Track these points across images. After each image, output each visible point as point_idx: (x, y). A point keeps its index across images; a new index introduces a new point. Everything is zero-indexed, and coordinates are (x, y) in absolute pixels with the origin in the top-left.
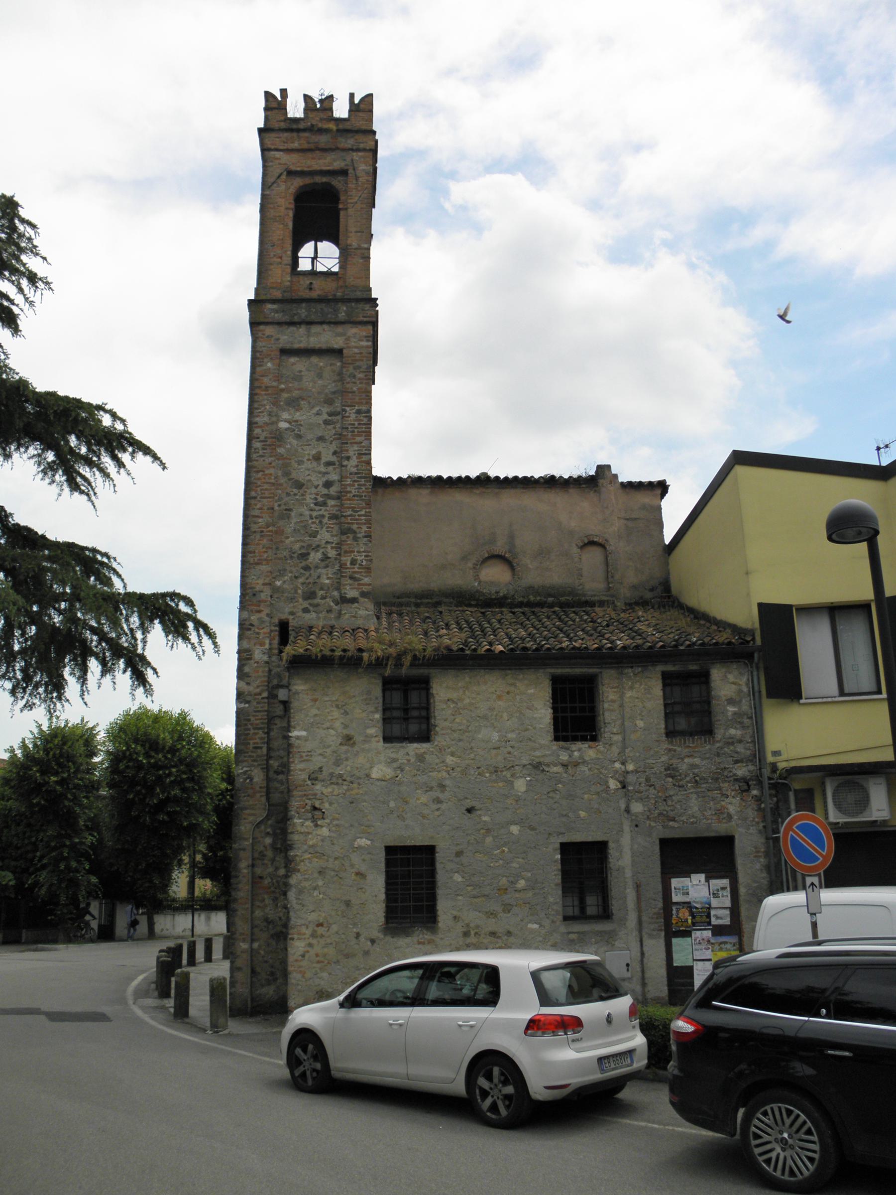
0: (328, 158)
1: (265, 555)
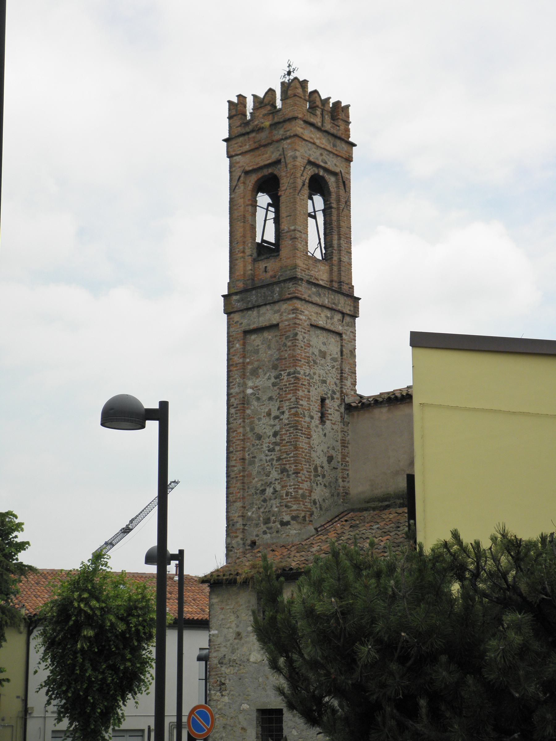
0: (269, 152)
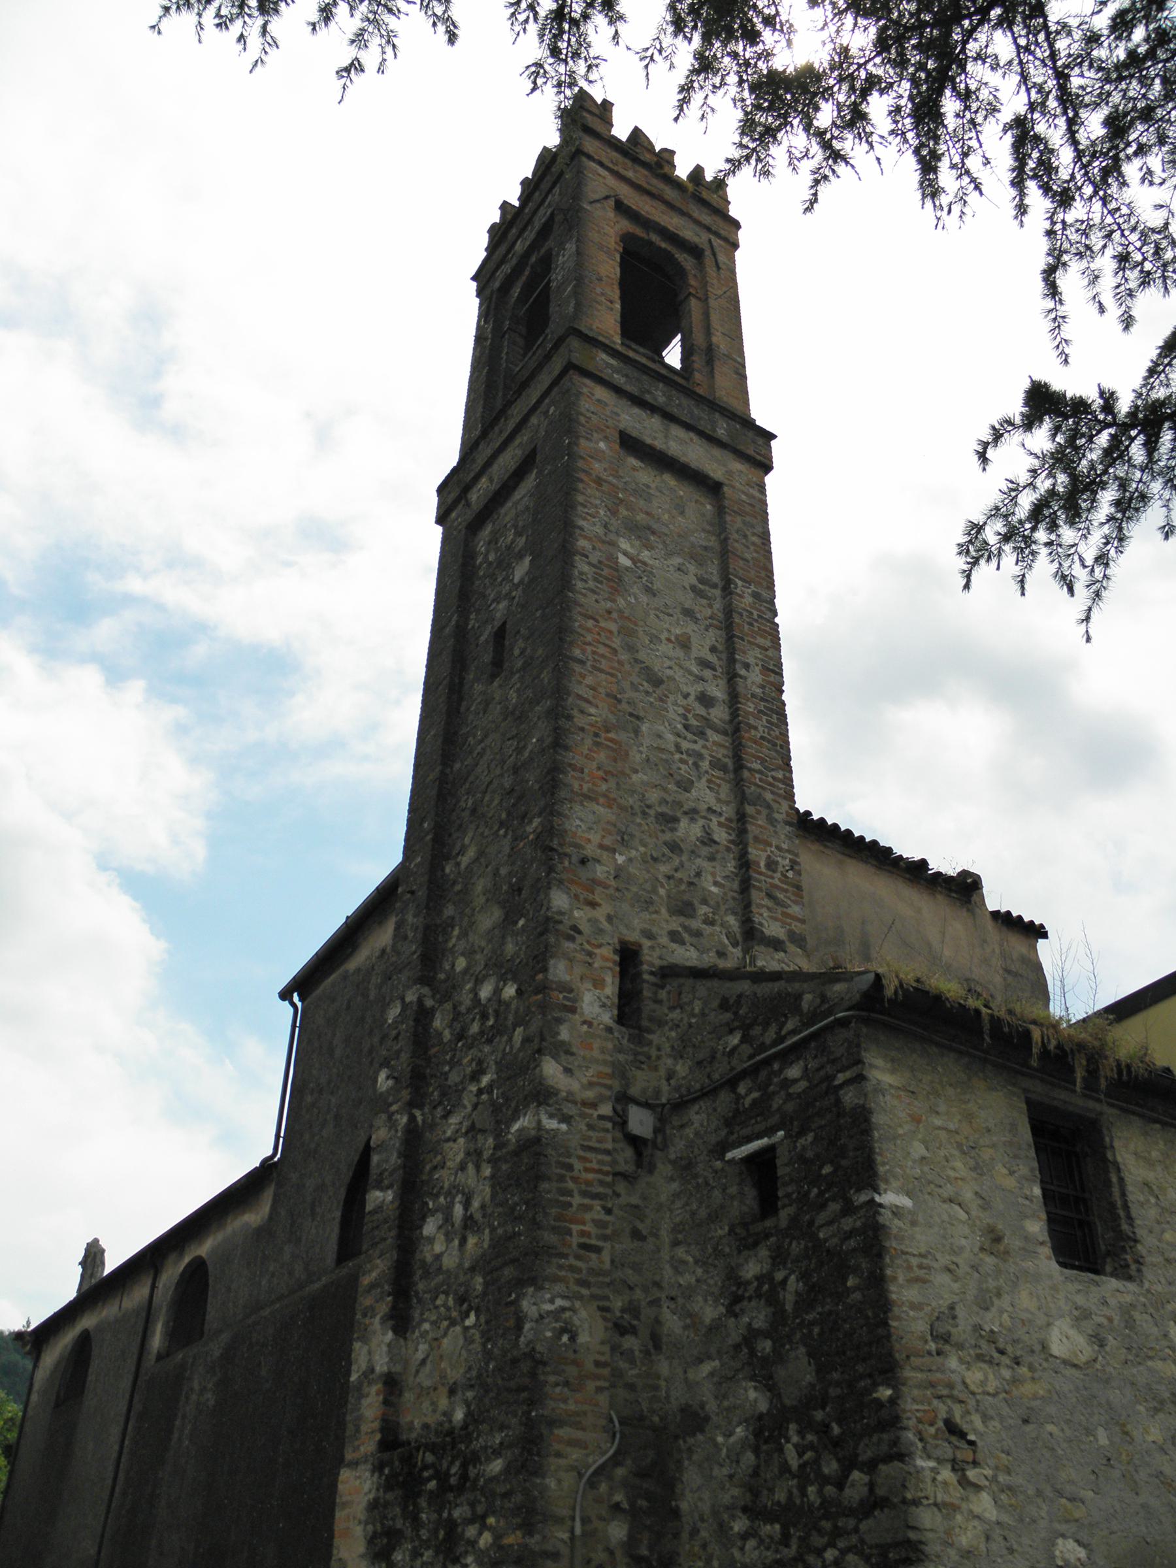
1: (604, 787)
